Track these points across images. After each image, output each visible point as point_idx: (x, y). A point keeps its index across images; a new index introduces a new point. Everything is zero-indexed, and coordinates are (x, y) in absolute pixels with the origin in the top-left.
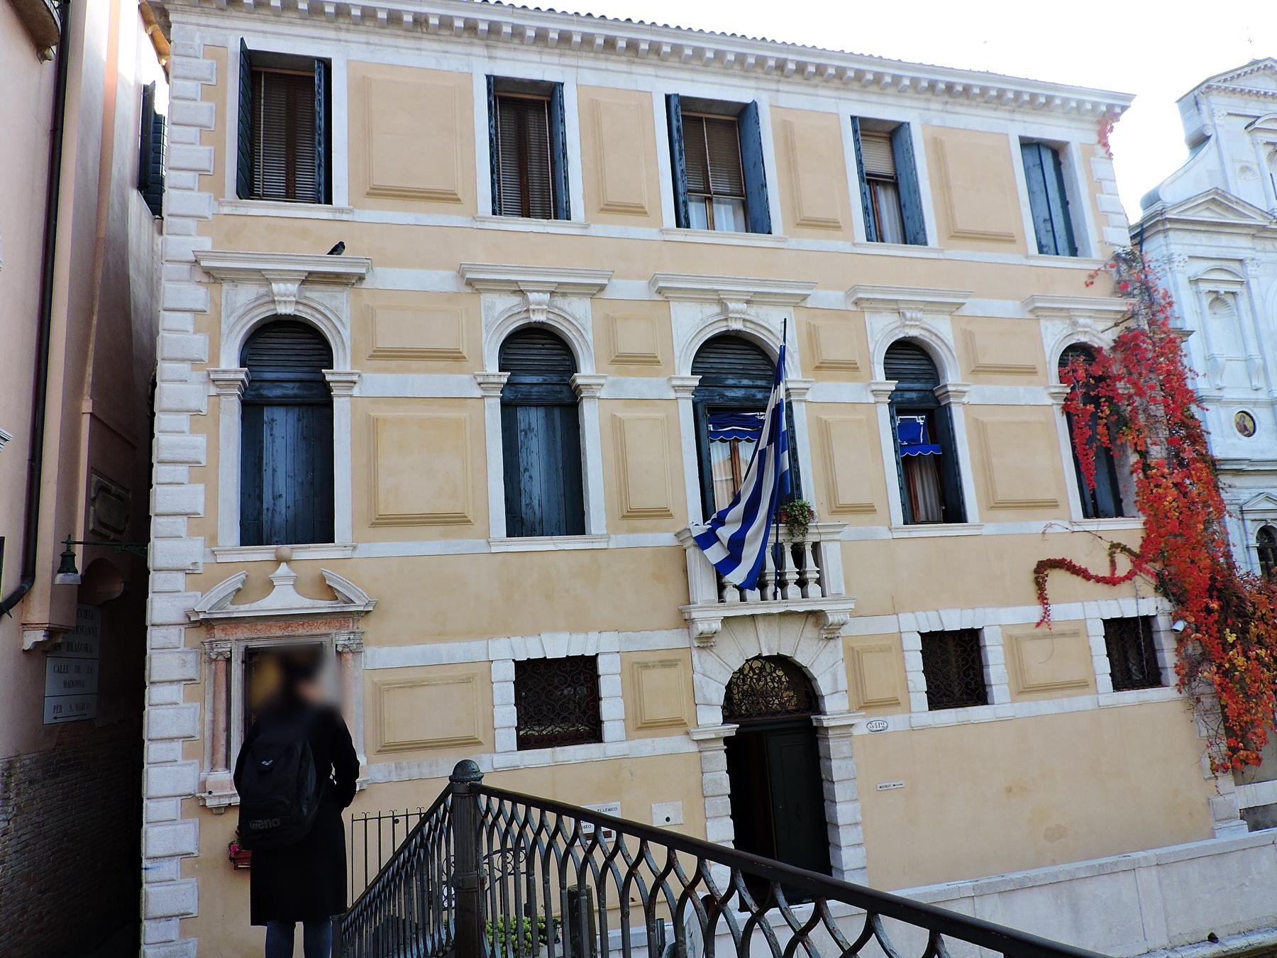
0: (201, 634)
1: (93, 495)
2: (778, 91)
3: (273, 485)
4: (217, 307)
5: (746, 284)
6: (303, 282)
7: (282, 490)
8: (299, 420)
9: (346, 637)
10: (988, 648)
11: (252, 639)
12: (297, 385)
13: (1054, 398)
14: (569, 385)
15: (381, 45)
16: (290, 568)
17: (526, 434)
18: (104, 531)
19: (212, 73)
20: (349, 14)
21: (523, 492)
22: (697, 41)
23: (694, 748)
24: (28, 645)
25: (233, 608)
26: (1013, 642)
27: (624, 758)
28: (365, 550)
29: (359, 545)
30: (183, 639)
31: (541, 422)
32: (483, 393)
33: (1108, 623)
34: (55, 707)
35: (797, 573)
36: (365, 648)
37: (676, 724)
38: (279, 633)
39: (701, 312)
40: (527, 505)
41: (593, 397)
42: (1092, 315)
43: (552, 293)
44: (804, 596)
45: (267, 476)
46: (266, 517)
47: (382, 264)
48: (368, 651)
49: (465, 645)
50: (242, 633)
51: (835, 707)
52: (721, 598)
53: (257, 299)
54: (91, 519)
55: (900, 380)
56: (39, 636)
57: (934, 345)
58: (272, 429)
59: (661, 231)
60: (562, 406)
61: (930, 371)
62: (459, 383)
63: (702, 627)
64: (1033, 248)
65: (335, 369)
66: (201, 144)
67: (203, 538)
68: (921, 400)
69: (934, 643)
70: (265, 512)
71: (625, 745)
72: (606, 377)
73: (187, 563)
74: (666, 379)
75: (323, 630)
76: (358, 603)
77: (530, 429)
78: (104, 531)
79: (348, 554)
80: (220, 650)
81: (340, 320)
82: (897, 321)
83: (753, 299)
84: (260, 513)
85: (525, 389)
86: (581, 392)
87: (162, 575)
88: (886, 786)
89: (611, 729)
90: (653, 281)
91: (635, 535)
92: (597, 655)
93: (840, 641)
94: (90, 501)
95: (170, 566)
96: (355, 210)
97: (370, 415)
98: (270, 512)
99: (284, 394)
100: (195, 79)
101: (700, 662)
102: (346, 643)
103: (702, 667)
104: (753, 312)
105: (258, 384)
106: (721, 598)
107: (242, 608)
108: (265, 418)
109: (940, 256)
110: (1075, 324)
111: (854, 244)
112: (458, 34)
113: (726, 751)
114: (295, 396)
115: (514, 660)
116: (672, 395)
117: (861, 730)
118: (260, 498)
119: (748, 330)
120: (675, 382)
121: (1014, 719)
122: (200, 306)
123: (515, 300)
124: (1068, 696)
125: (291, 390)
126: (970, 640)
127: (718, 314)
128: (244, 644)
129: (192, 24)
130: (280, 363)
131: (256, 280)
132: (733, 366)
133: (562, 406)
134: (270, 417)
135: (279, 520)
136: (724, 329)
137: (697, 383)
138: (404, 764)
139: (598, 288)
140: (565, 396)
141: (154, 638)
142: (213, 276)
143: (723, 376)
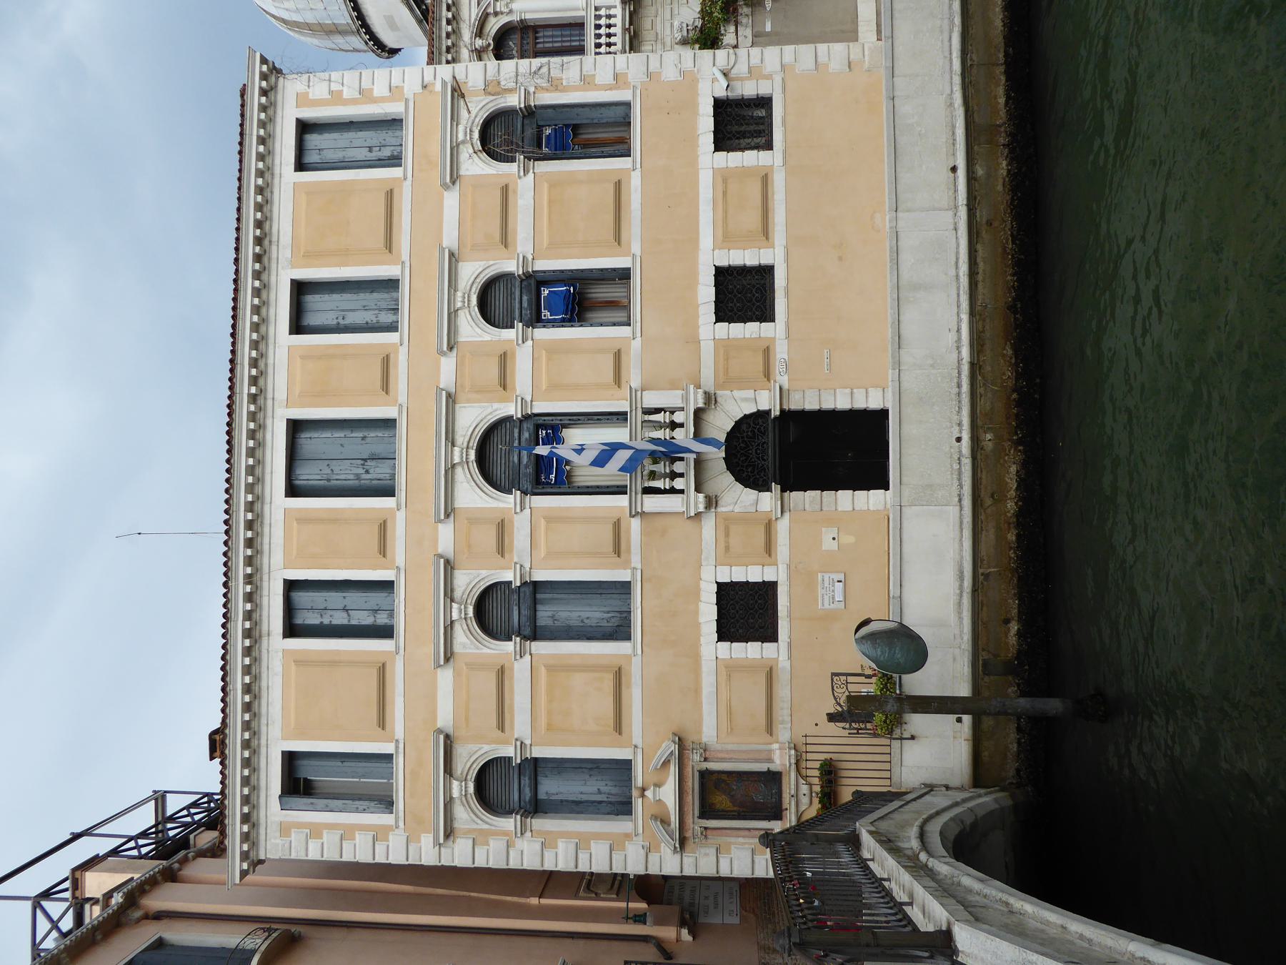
0: (690, 845)
1: (594, 895)
2: (273, 399)
3: (591, 794)
4: (470, 831)
5: (440, 447)
6: (451, 775)
7: (595, 789)
8: (546, 776)
9: (695, 754)
10: (731, 263)
11: (693, 814)
12: (522, 777)
13: (528, 171)
14: (521, 421)
15: (278, 242)
16: (647, 790)
17: (556, 620)
18: (616, 886)
19: (302, 832)
20: (250, 630)
21: (598, 624)
22: (234, 875)
23: (787, 515)
24: (690, 938)
25: (673, 825)
26: (726, 555)
27: (789, 567)
28: (637, 739)
29: (633, 743)
30: (691, 855)
31: (547, 608)
32: (528, 831)
33: (719, 319)
34: (730, 915)
35: (665, 413)
36: (703, 742)
37: (769, 527)
38: (691, 797)
39: (462, 483)
40: (608, 622)
41: (530, 573)
42: (455, 123)
43: (452, 600)
44: (681, 425)
45: (585, 798)
46: (613, 799)
47: (437, 550)
48: (704, 740)
49: (704, 675)
50: (689, 820)
51: (766, 401)
52: (682, 492)
53: (464, 805)
54: (609, 896)
55: (514, 319)
56: (685, 932)
57: (484, 280)
58: (553, 794)
59: (398, 510)
60: (535, 593)
61: (505, 283)
62: (521, 670)
63: (701, 508)
64: (395, 172)
65: (512, 579)
66: (354, 839)
67: (627, 842)
68: (530, 291)
69: (725, 312)
70: (610, 800)
71: (780, 566)
72: (518, 254)
73: (642, 852)
74: (519, 180)
75: (690, 770)
76: (673, 748)
77: (553, 617)
78: (616, 886)
79: (639, 751)
80: (699, 834)
81: (477, 751)
82: (465, 313)
83: (451, 440)
84: (610, 803)
85: (523, 619)
86: (530, 106)
87: (650, 866)
88: (827, 365)
89: (769, 576)
90: (442, 353)
91: (632, 548)
92: (716, 582)
93: (718, 392)
94: (597, 898)
95: (644, 862)
96: (396, 738)
97: (546, 390)
98: (610, 796)
99: (529, 786)
100: (307, 843)
101: (726, 506)
102: (699, 755)
103: (730, 505)
104: (461, 439)
105: (522, 803)
106: (682, 492)
107: (673, 819)
108: (546, 798)
109: (407, 265)
110: (463, 142)
111: (405, 179)
112: (256, 660)
113: (791, 491)
114: (530, 779)
115: (715, 323)
116: (527, 511)
117: (784, 380)
118: (600, 802)
119: (475, 445)
120: (518, 510)
121: (786, 248)
122: (470, 842)
123: (459, 470)
124: (773, 194)
125: (526, 781)
126: (724, 276)
127: (463, 469)
128: (696, 819)
129: (266, 844)
130: (507, 793)
131: (451, 806)
132: (503, 455)
133: (535, 593)
134: (545, 795)
135: (614, 791)
136: (475, 464)
137: (521, 324)
138: (780, 719)
139: (447, 565)
140: (528, 591)
141: (689, 871)
142: (449, 833)
143: (511, 464)
